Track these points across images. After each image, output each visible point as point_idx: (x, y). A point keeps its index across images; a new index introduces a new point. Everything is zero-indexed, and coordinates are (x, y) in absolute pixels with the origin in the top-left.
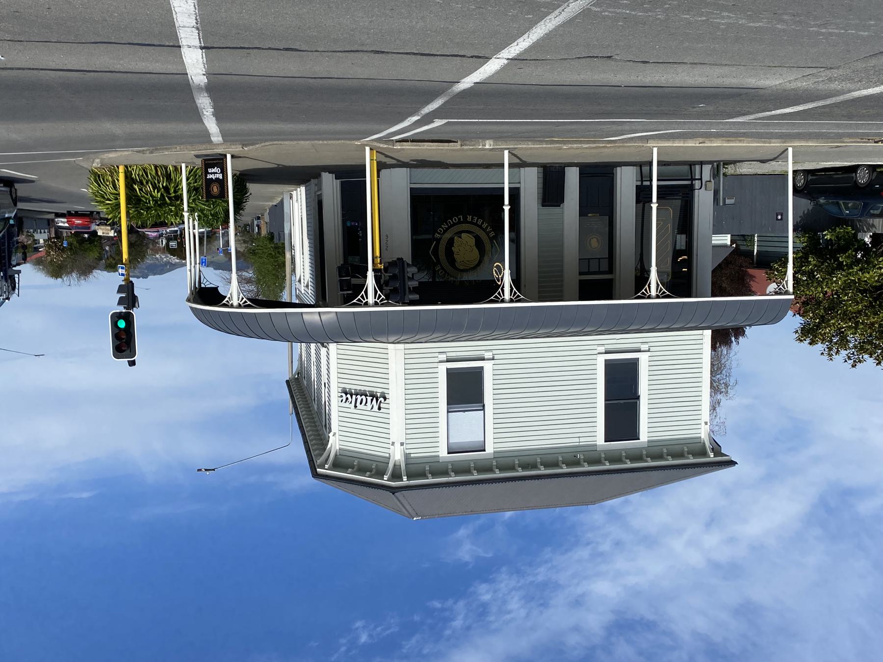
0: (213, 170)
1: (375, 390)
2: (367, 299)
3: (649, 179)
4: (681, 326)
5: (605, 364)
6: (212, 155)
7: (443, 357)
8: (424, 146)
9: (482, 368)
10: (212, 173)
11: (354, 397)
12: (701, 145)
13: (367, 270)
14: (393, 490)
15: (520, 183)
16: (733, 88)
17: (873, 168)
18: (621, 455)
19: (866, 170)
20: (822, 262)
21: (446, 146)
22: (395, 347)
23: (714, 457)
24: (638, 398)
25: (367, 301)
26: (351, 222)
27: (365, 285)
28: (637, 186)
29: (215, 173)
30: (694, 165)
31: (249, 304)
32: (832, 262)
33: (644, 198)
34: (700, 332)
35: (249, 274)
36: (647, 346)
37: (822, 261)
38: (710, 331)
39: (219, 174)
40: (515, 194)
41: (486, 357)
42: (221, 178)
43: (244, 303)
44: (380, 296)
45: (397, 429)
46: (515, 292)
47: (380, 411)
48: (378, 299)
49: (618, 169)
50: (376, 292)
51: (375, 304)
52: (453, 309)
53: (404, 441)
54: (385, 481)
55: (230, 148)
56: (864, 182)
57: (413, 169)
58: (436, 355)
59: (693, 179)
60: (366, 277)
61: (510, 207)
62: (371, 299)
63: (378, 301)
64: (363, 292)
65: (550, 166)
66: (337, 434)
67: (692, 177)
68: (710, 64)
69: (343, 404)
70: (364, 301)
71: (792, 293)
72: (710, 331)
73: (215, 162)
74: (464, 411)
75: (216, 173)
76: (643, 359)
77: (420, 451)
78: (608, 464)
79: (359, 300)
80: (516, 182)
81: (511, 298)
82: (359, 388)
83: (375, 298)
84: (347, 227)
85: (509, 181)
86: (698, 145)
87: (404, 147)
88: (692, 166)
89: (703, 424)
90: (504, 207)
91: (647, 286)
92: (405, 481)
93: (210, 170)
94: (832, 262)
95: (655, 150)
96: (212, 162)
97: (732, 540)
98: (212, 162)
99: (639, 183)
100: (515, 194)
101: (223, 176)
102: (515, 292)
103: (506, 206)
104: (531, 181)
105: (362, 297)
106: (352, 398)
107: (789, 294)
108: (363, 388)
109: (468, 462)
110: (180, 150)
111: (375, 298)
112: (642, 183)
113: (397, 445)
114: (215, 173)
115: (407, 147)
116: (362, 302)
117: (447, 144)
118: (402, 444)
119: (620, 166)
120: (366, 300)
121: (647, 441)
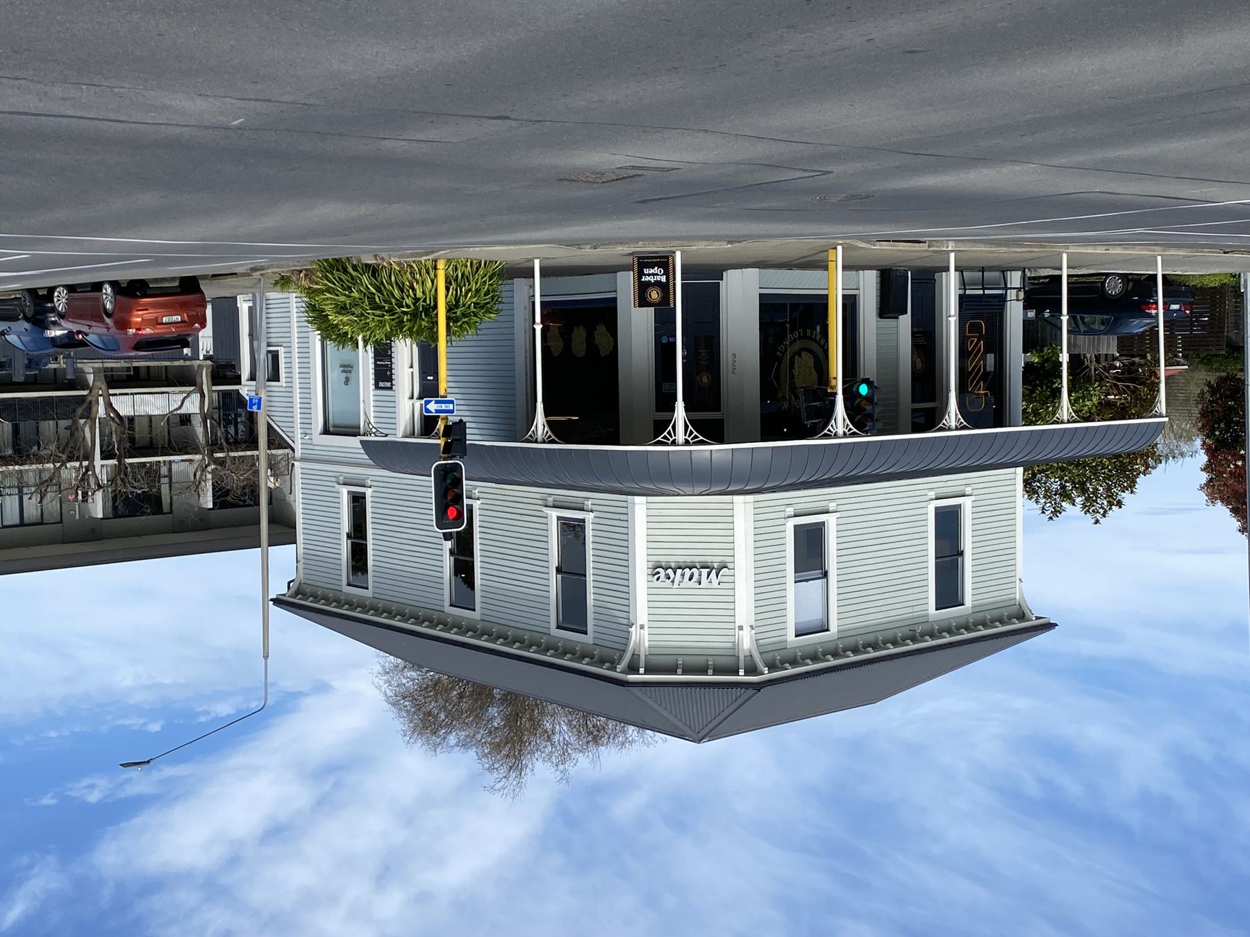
0: (652, 271)
1: (709, 559)
2: (675, 436)
3: (981, 287)
4: (778, 483)
5: (936, 514)
6: (656, 252)
7: (790, 511)
8: (898, 246)
9: (823, 523)
10: (649, 275)
11: (679, 571)
12: (1107, 252)
13: (675, 399)
14: (758, 687)
15: (858, 289)
16: (26, 114)
17: (1124, 277)
18: (796, 656)
19: (1118, 280)
20: (1032, 389)
21: (916, 247)
22: (745, 499)
23: (769, 673)
24: (961, 554)
25: (675, 439)
26: (668, 337)
27: (672, 420)
28: (959, 295)
29: (654, 275)
30: (1007, 271)
31: (702, 440)
32: (1045, 389)
33: (968, 309)
34: (1013, 470)
35: (1071, 378)
36: (835, 504)
37: (1030, 388)
38: (1022, 468)
39: (661, 275)
40: (850, 304)
41: (831, 509)
42: (665, 281)
43: (548, 438)
44: (691, 433)
45: (745, 611)
46: (664, 438)
47: (700, 586)
48: (689, 437)
49: (1009, 272)
50: (686, 427)
51: (685, 443)
52: (868, 442)
53: (753, 623)
54: (741, 677)
55: (712, 245)
56: (1115, 292)
57: (765, 271)
58: (783, 508)
59: (1006, 288)
60: (673, 410)
61: (542, 326)
62: (681, 437)
63: (689, 439)
64: (670, 428)
65: (897, 270)
66: (646, 628)
67: (1006, 285)
68: (712, 132)
69: (658, 584)
70: (671, 440)
71: (954, 428)
72: (1022, 468)
73: (654, 260)
74: (807, 581)
75: (657, 274)
76: (831, 521)
77: (770, 639)
78: (948, 636)
79: (665, 437)
80: (854, 288)
81: (686, 439)
82: (681, 559)
83: (685, 435)
84: (662, 343)
85: (843, 286)
86: (1104, 252)
87: (883, 247)
88: (1005, 273)
89: (1018, 581)
90: (1062, 318)
91: (833, 420)
92: (767, 675)
93: (646, 271)
94: (1045, 389)
95: (1065, 256)
96: (650, 260)
97: (423, 898)
98: (650, 260)
99: (961, 292)
100: (850, 304)
101: (668, 279)
102: (664, 438)
103: (538, 324)
104: (868, 285)
105: (669, 433)
106: (675, 574)
107: (1163, 417)
108: (689, 559)
109: (835, 642)
110: (642, 246)
111: (685, 435)
112: (965, 292)
113: (747, 629)
114: (654, 275)
115: (887, 248)
116: (669, 440)
117: (917, 245)
118: (752, 627)
119: (1011, 271)
120: (674, 438)
121: (971, 606)
